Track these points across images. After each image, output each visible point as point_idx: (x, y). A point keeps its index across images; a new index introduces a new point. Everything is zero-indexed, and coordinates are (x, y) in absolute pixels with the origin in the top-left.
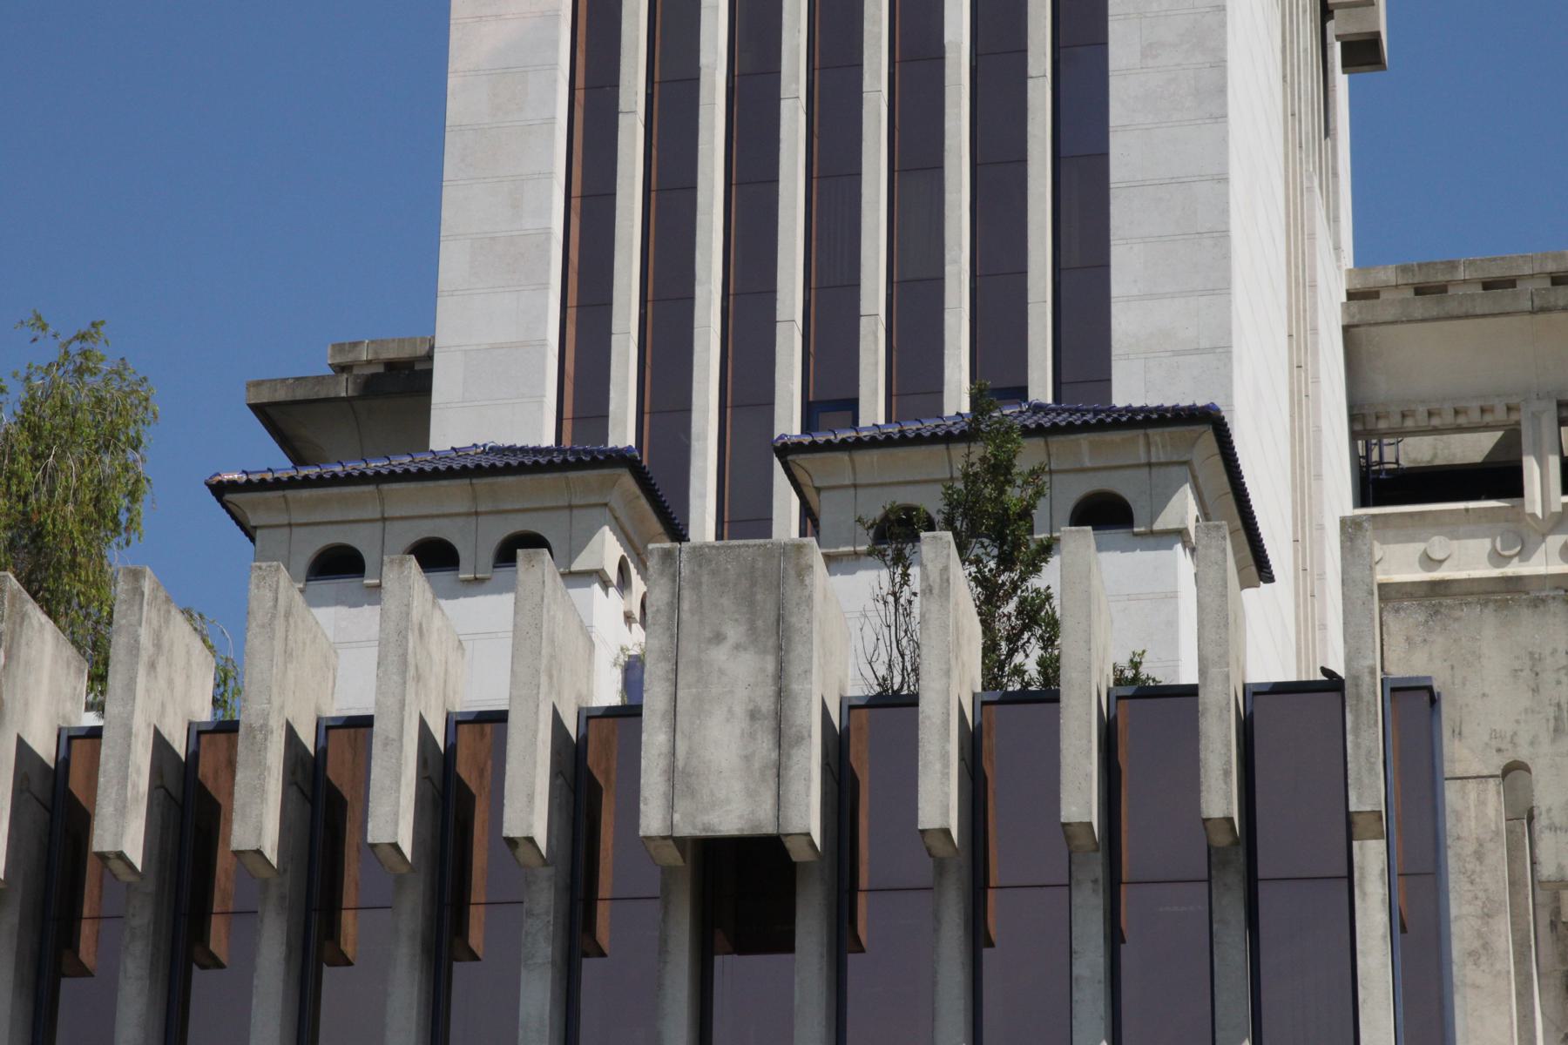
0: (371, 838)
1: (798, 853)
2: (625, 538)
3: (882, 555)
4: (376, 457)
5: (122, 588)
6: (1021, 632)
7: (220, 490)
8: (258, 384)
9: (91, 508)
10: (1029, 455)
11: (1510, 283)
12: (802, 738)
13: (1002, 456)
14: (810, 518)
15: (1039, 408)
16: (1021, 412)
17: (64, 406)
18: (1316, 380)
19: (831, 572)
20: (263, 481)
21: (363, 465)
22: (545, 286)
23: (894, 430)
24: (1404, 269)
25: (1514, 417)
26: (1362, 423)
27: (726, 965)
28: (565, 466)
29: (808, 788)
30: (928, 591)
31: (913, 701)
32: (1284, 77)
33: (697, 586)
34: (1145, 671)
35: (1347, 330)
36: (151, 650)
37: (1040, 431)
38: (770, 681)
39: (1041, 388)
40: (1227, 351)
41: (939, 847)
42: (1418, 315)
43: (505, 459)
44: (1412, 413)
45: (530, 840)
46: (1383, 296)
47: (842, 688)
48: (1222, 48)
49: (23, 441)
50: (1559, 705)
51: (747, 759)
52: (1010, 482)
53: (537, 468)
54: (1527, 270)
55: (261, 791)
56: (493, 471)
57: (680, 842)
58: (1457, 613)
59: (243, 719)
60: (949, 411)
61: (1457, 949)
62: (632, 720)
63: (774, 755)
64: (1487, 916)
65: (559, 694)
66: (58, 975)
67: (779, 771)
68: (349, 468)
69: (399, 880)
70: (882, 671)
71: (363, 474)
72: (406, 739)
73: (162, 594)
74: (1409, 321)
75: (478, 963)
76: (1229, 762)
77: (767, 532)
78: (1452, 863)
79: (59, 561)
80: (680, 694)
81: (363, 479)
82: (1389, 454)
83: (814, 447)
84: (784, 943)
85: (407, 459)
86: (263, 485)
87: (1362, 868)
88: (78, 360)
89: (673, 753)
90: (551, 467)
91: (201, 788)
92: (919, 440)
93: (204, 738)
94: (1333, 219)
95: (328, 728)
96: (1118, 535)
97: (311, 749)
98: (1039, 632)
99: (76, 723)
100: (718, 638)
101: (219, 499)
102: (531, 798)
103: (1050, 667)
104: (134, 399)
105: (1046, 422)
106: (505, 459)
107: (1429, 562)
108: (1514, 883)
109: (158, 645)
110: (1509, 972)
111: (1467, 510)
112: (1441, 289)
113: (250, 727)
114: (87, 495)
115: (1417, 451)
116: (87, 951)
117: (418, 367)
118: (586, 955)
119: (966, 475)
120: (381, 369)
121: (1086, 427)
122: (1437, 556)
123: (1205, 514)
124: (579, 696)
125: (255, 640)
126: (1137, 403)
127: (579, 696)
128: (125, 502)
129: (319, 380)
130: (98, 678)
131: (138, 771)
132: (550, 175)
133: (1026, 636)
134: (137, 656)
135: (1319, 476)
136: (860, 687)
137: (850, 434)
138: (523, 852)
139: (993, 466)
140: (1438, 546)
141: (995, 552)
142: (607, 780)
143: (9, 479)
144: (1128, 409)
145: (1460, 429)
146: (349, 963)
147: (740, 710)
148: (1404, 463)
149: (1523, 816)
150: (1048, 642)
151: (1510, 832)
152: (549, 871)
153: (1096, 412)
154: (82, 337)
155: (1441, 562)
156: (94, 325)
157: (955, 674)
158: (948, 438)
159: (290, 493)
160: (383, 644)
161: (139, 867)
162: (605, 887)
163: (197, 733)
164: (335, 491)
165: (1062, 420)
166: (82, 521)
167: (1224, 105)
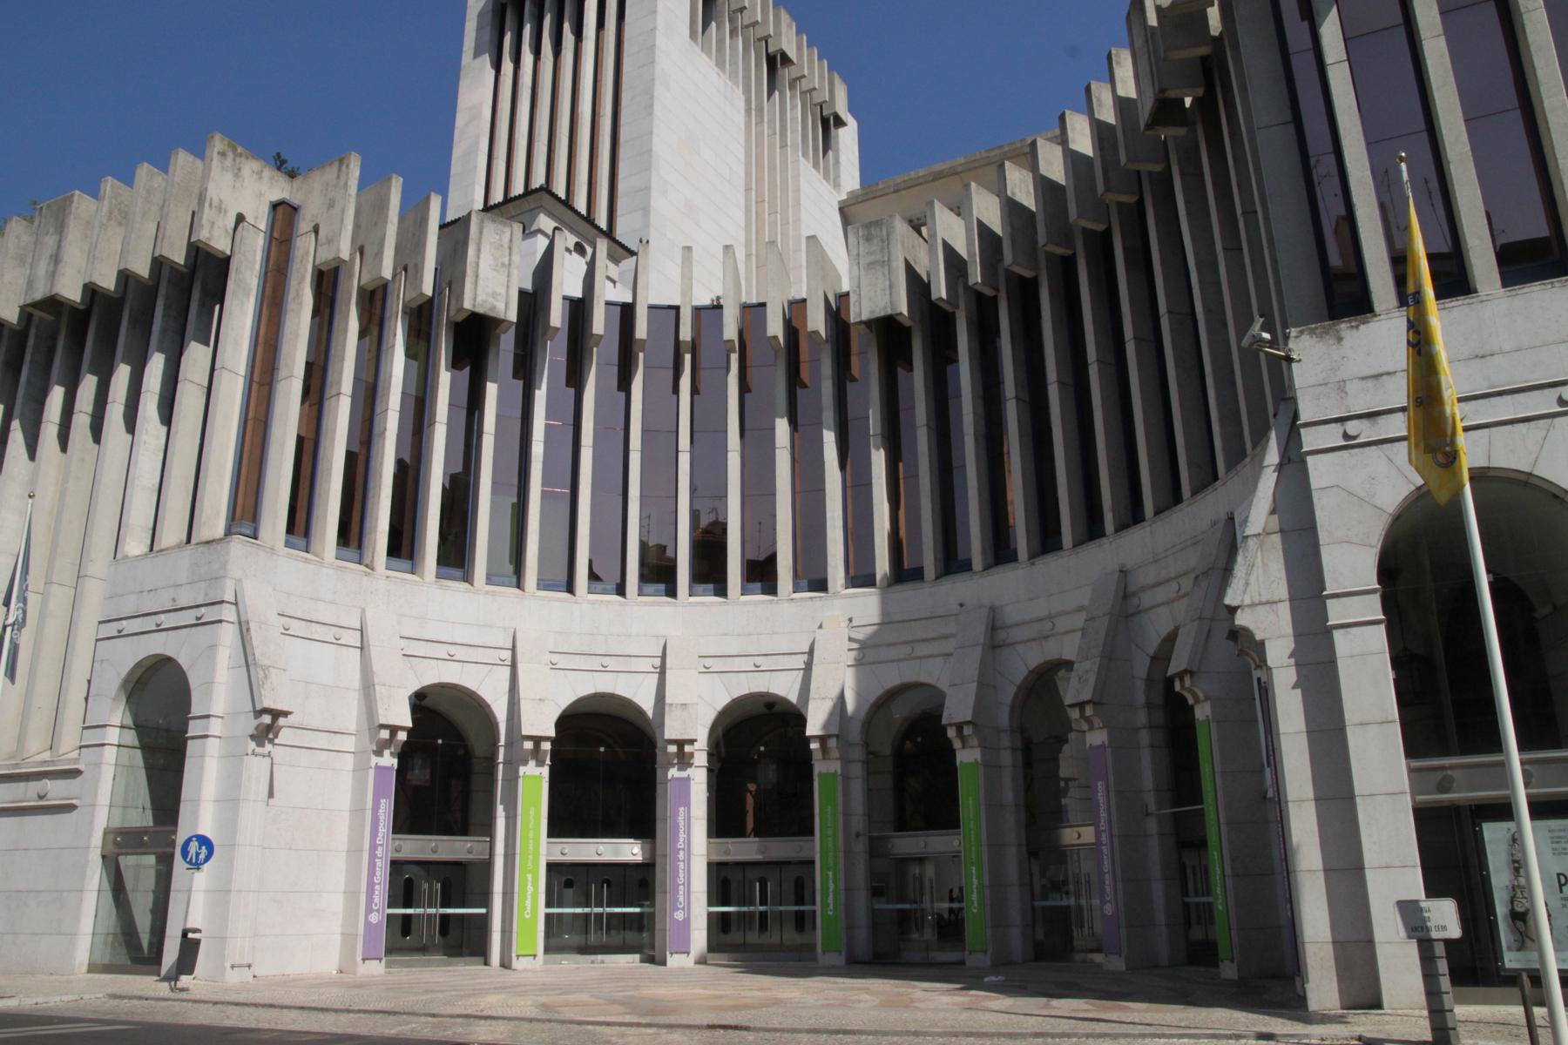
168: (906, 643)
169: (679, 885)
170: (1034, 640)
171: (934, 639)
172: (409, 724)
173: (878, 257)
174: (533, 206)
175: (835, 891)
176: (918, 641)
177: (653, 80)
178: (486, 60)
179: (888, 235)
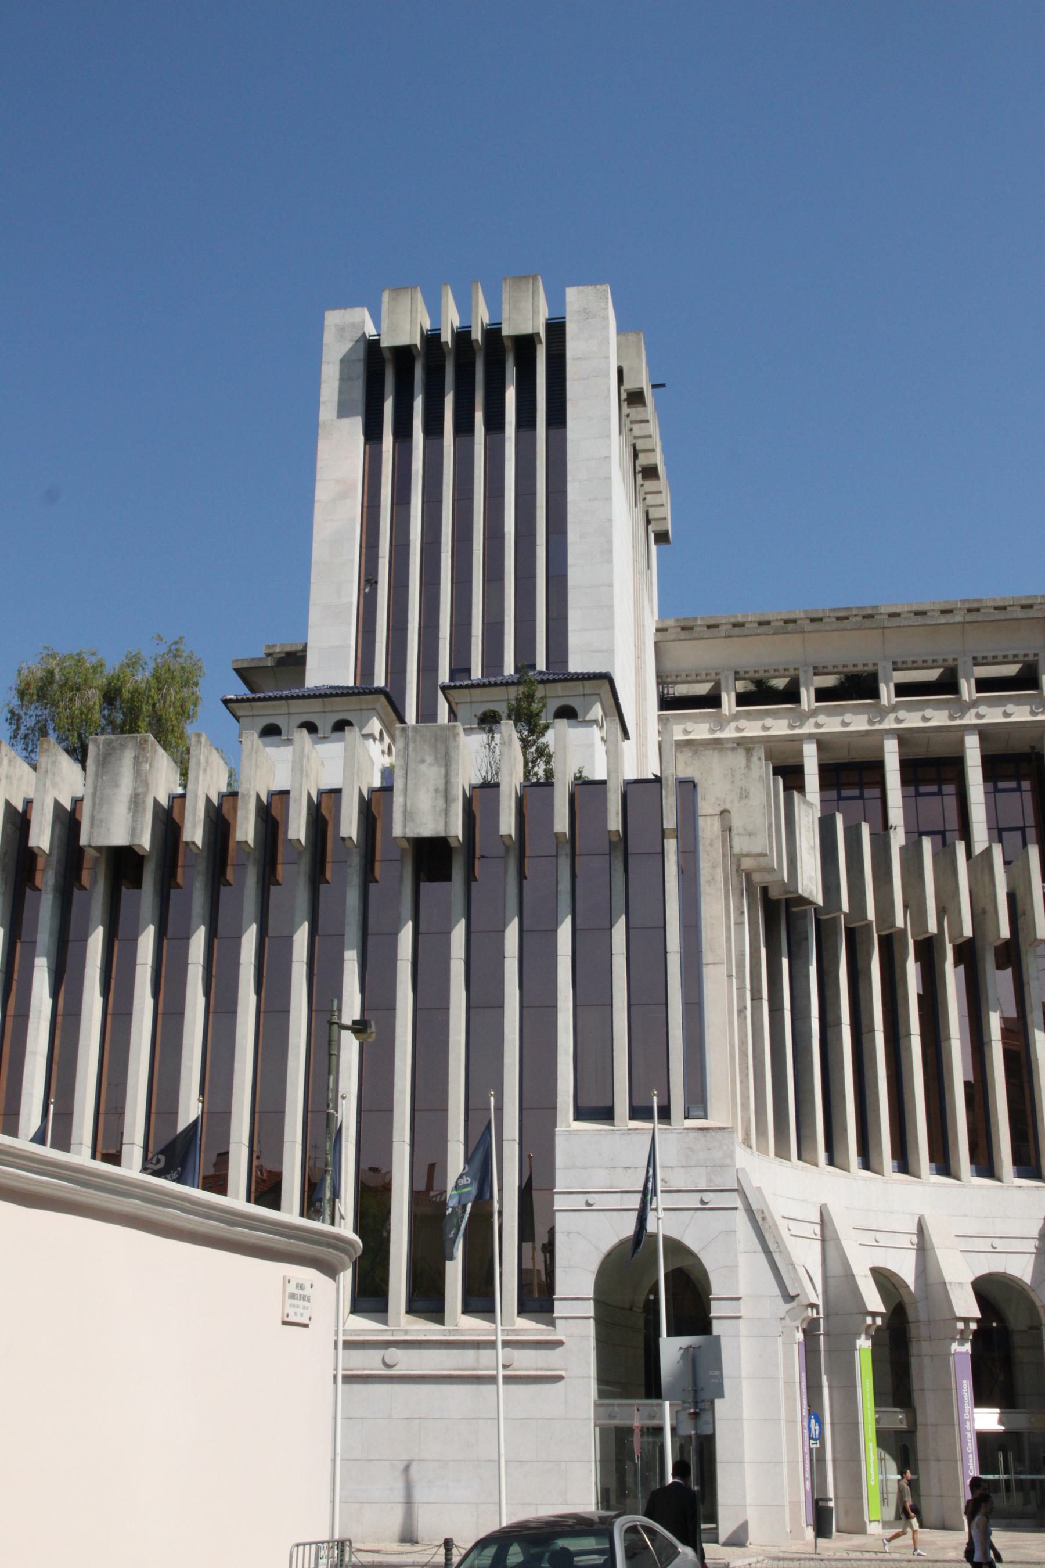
0: (290, 837)
1: (453, 844)
2: (382, 721)
3: (484, 729)
4: (285, 690)
5: (194, 740)
6: (537, 759)
7: (226, 702)
8: (237, 661)
9: (179, 709)
10: (540, 691)
11: (716, 626)
12: (454, 800)
13: (531, 692)
14: (453, 714)
15: (541, 673)
16: (535, 674)
17: (169, 670)
18: (644, 662)
19: (466, 735)
20: (242, 699)
21: (281, 693)
22: (350, 624)
23: (485, 680)
24: (678, 620)
25: (718, 677)
26: (662, 680)
27: (424, 886)
28: (359, 694)
29: (457, 819)
30: (503, 743)
31: (497, 785)
32: (633, 546)
33: (415, 741)
34: (584, 774)
35: (656, 643)
36: (205, 764)
37: (542, 682)
38: (443, 778)
39: (541, 664)
40: (613, 651)
41: (508, 842)
43: (336, 691)
44: (680, 676)
45: (351, 838)
46: (669, 630)
47: (470, 780)
48: (611, 535)
49: (154, 683)
50: (741, 788)
51: (434, 807)
52: (534, 702)
53: (348, 694)
54: (723, 621)
55: (247, 819)
56: (331, 695)
57: (408, 839)
58: (704, 753)
59: (240, 790)
62: (550, 788)
63: (444, 806)
64: (714, 867)
65: (361, 783)
66: (169, 888)
67: (446, 812)
68: (275, 694)
69: (300, 853)
70: (484, 774)
71: (281, 696)
72: (303, 799)
73: (209, 743)
74: (679, 640)
75: (328, 885)
76: (618, 810)
77: (435, 720)
79: (167, 729)
80: (408, 782)
81: (281, 698)
82: (671, 691)
83: (455, 687)
84: (448, 878)
85: (297, 691)
86: (242, 701)
87: (668, 850)
88: (175, 652)
89: (406, 805)
90: (354, 694)
91: (223, 817)
92: (496, 685)
93: (224, 798)
94: (651, 601)
95: (272, 795)
96: (573, 721)
97: (265, 802)
98: (544, 759)
99: (175, 792)
100: (423, 761)
101: (226, 706)
102: (351, 823)
103: (549, 774)
104: (196, 667)
105: (545, 678)
106: (336, 691)
108: (724, 855)
109: (207, 762)
110: (721, 889)
111: (700, 713)
112: (691, 628)
113: (243, 795)
114: (178, 704)
115: (681, 690)
116: (180, 879)
117: (299, 654)
118: (371, 882)
119: (516, 699)
120: (284, 655)
121: (560, 680)
122: (689, 730)
123: (605, 714)
124: (369, 783)
125: (245, 761)
126: (579, 671)
127: (369, 783)
128: (192, 707)
129: (260, 659)
130: (184, 774)
131: (200, 810)
132: (352, 581)
133: (539, 760)
134: (199, 766)
135: (645, 699)
136: (477, 780)
137: (469, 682)
138: (348, 842)
139: (528, 695)
141: (527, 728)
142: (379, 815)
143: (148, 698)
144: (576, 674)
145: (698, 682)
146: (280, 885)
147: (431, 788)
148: (677, 694)
149: (728, 830)
150: (548, 763)
151: (722, 836)
152: (358, 850)
153: (564, 674)
154: (176, 643)
155: (690, 732)
156: (180, 638)
157: (514, 775)
158: (507, 684)
159: (253, 704)
160: (294, 762)
161: (201, 847)
162: (378, 857)
163: (222, 796)
164: (270, 703)
165: (551, 677)
166: (176, 714)
167: (611, 557)
169: (969, 1454)
172: (977, 1314)
174: (587, 691)
177: (610, 520)
178: (355, 426)
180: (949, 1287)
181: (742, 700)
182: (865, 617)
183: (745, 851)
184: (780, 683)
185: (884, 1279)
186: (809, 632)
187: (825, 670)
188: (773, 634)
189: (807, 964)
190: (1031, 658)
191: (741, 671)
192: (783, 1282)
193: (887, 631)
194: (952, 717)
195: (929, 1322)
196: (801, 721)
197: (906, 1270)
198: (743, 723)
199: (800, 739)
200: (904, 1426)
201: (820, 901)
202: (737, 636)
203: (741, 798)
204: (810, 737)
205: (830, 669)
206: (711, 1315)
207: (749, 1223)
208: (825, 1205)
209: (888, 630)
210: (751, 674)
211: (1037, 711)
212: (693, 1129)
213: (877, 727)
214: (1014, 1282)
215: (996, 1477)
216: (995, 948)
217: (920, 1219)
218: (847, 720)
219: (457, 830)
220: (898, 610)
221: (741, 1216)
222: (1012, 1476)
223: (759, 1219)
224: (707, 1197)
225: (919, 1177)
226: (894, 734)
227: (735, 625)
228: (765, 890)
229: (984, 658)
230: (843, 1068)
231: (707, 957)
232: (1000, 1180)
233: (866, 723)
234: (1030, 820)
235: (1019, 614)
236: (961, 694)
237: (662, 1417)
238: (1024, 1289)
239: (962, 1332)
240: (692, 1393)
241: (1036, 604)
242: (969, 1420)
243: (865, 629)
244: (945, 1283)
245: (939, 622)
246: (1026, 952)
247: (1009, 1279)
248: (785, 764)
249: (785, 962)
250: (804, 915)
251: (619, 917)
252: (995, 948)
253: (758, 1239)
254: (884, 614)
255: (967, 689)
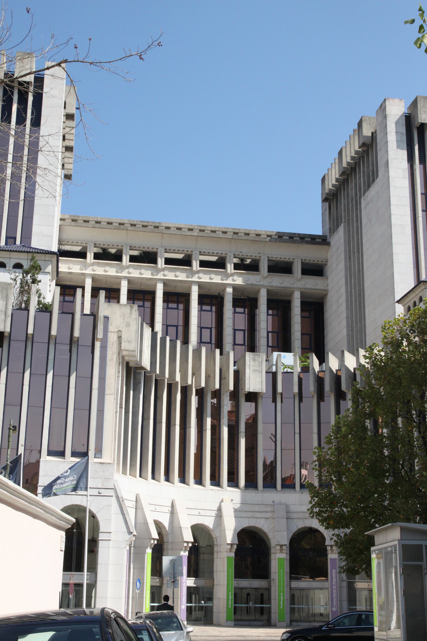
24: (70, 216)
25: (86, 245)
35: (60, 225)
38: (4, 306)
42: (73, 225)
46: (66, 220)
54: (91, 220)
60: (230, 389)
61: (108, 359)
63: (4, 318)
64: (113, 354)
67: (5, 321)
78: (108, 345)
107: (69, 268)
122: (71, 267)
140: (71, 266)
145: (77, 246)
148: (65, 249)
168: (251, 512)
169: (183, 595)
170: (301, 519)
171: (262, 512)
172: (192, 540)
173: (257, 368)
174: (47, 259)
175: (283, 600)
176: (256, 512)
179: (261, 361)
180: (182, 529)
181: (97, 256)
182: (155, 227)
183: (126, 349)
184: (113, 251)
185: (158, 524)
186: (130, 230)
187: (135, 248)
188: (114, 229)
189: (139, 393)
190: (224, 255)
191: (97, 243)
192: (128, 526)
193: (164, 235)
194: (187, 277)
195: (172, 543)
196: (122, 270)
197: (166, 522)
198: (95, 268)
199: (121, 278)
200: (158, 584)
201: (148, 368)
202: (98, 228)
203: (126, 326)
204: (125, 277)
205: (137, 248)
206: (99, 539)
207: (117, 502)
208: (138, 494)
209: (165, 234)
210: (102, 246)
211: (224, 279)
212: (98, 463)
213: (155, 277)
214: (205, 527)
215: (191, 605)
216: (212, 391)
217: (173, 500)
218: (142, 272)
219: (8, 330)
220: (170, 226)
221: (114, 499)
222: (197, 605)
223: (121, 500)
224: (101, 491)
225: (173, 484)
226: (162, 281)
227: (97, 222)
228: (128, 363)
229: (204, 252)
230: (149, 437)
231: (107, 391)
232: (204, 486)
233: (150, 275)
234: (214, 326)
235: (222, 235)
236: (192, 267)
237: (83, 579)
238: (209, 531)
239: (185, 547)
240: (173, 575)
241: (229, 232)
242: (185, 582)
243: (155, 232)
244: (181, 527)
245: (187, 234)
246: (224, 394)
247: (204, 526)
248: (112, 287)
249: (132, 392)
250: (140, 373)
251: (73, 373)
252: (212, 391)
253: (120, 509)
254: (164, 226)
255: (195, 265)
